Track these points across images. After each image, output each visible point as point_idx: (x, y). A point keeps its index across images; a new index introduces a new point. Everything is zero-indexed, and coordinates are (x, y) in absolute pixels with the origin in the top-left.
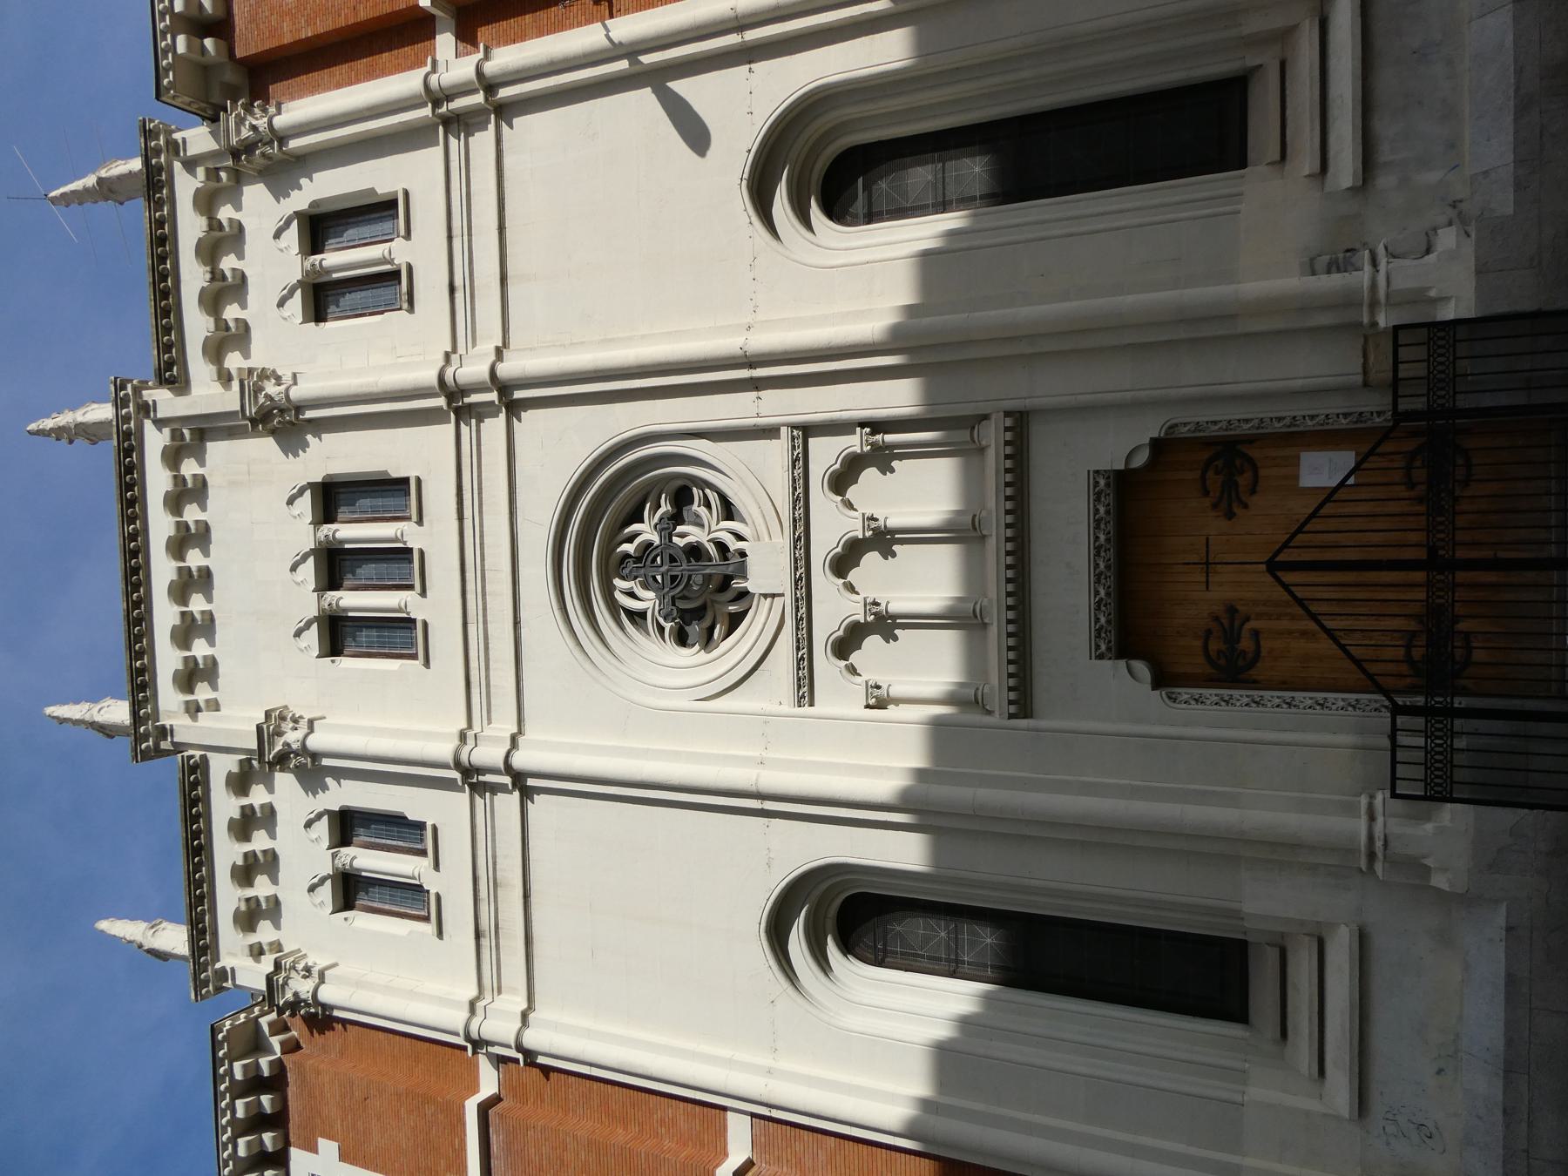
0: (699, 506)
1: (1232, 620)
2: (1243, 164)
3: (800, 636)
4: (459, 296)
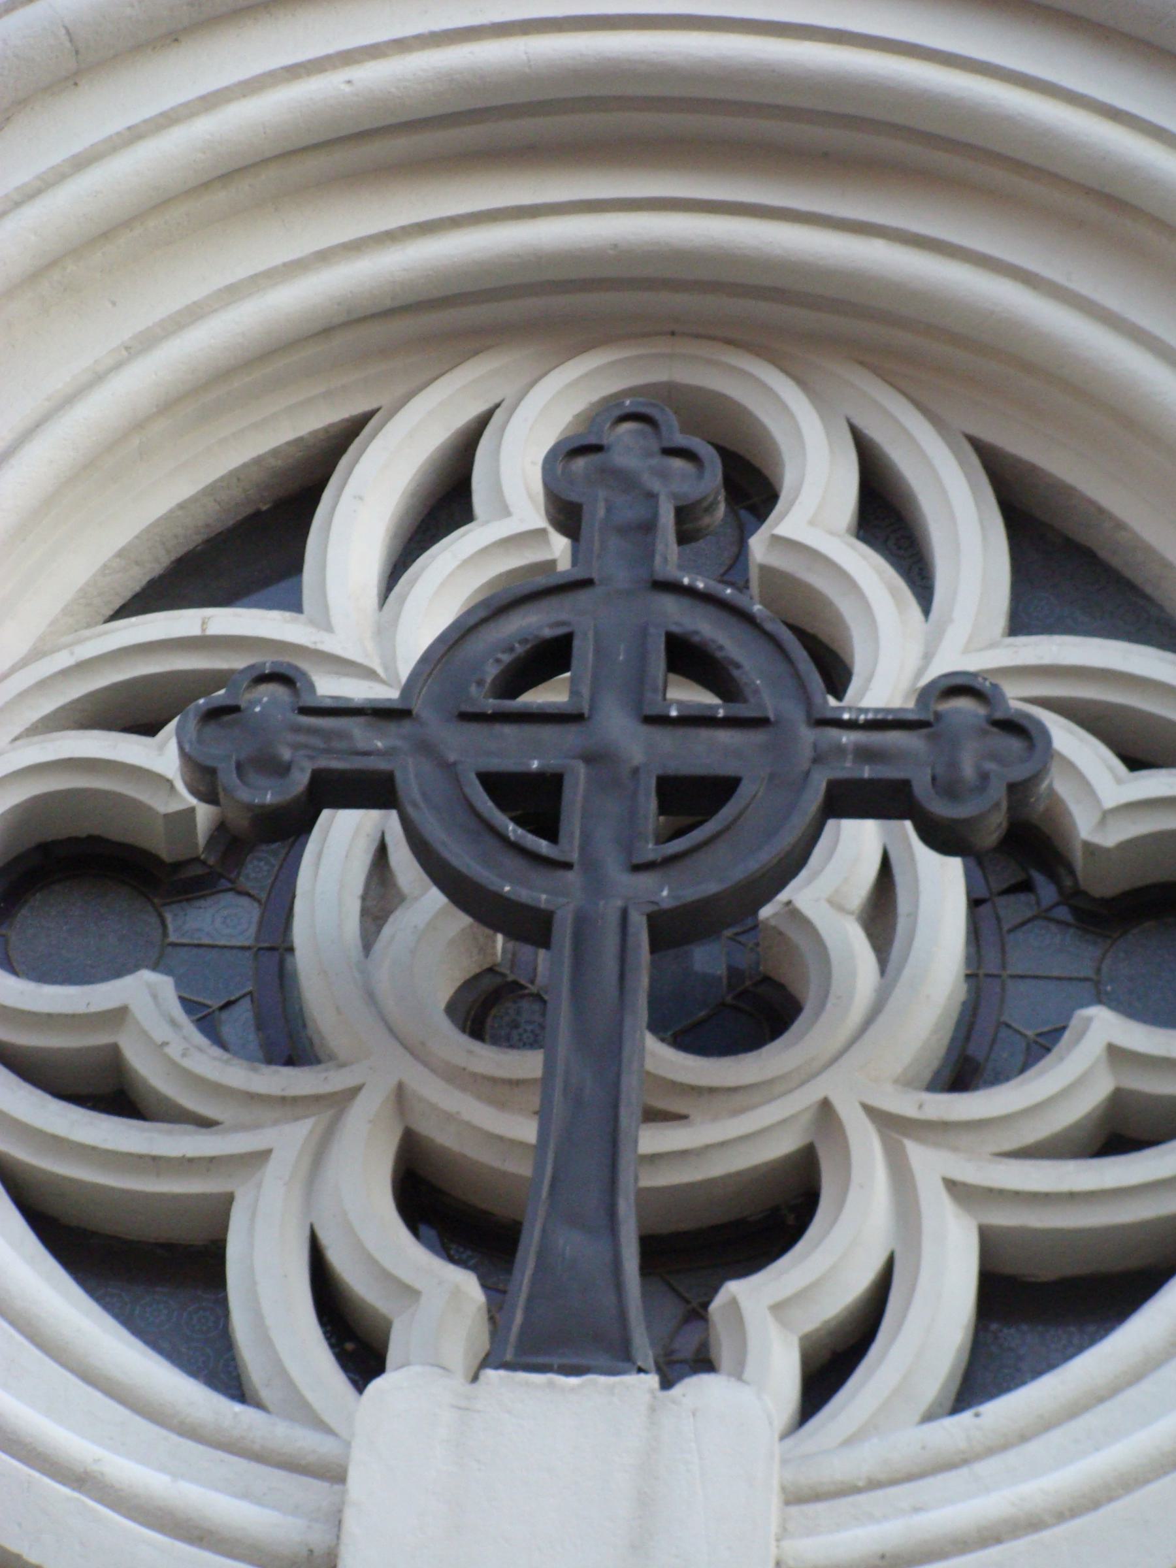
0: (1116, 1054)
3: (262, 864)
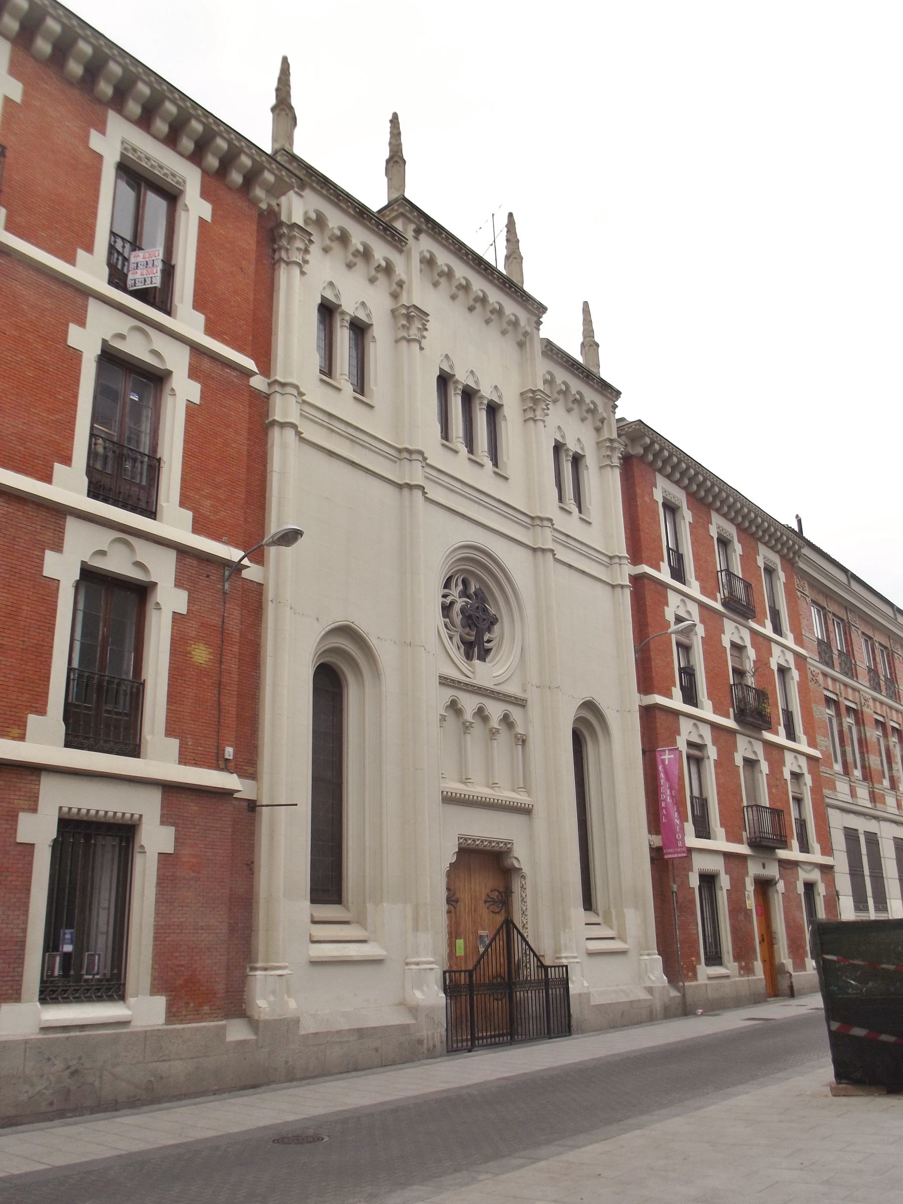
1: (489, 902)
2: (313, 901)
4: (325, 418)
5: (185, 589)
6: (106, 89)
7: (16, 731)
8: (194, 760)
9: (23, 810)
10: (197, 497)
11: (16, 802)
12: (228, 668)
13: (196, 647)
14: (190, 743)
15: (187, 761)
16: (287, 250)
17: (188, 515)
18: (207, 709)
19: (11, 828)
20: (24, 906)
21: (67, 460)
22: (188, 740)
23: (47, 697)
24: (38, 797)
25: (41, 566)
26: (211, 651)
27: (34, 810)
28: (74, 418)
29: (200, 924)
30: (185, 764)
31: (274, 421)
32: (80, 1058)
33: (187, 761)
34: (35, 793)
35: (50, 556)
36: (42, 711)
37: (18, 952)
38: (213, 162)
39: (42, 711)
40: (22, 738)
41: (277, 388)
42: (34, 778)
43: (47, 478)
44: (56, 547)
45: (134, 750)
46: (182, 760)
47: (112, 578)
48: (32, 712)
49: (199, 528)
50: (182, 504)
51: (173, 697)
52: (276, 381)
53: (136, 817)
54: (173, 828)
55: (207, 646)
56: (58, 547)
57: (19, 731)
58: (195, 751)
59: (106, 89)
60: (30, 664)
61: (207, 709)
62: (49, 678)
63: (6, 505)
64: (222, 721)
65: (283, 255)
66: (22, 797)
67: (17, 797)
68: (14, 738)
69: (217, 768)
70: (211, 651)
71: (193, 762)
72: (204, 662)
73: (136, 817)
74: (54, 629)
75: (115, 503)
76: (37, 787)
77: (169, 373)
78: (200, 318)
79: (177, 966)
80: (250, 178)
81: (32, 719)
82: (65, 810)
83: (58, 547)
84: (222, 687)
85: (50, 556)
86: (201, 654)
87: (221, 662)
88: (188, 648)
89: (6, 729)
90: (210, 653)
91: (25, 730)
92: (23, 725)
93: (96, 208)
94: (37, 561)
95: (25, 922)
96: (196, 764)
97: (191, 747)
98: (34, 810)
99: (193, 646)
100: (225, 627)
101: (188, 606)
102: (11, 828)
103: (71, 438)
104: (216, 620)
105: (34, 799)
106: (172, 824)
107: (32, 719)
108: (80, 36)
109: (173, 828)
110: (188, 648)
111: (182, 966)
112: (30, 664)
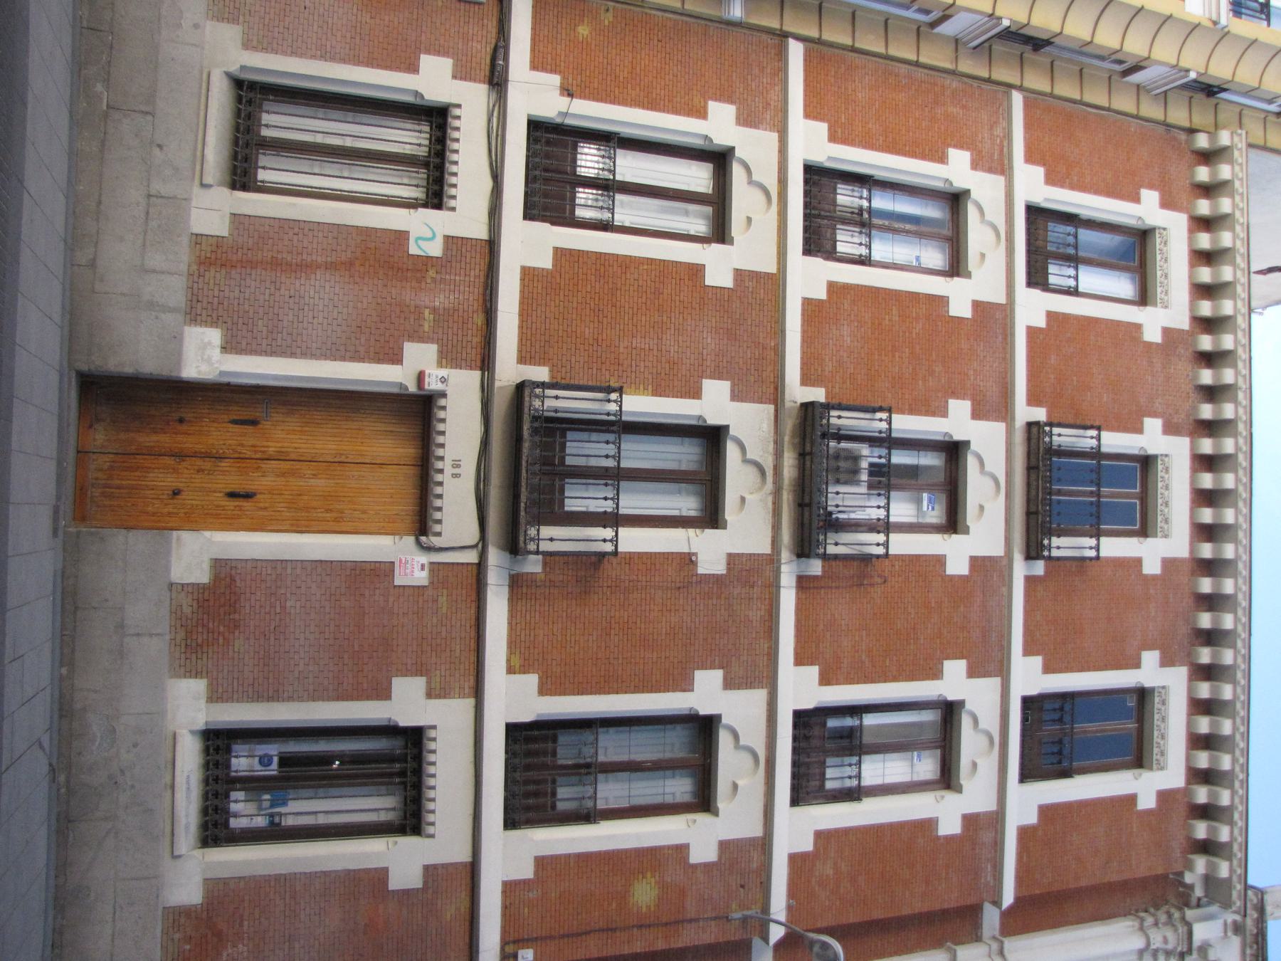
5: (720, 857)
6: (1205, 655)
7: (516, 662)
8: (510, 904)
9: (429, 682)
10: (833, 855)
11: (438, 672)
12: (635, 937)
13: (653, 885)
14: (531, 895)
15: (508, 894)
16: (1156, 924)
17: (807, 845)
18: (578, 914)
19: (407, 670)
20: (317, 695)
21: (825, 680)
22: (535, 892)
23: (560, 694)
24: (445, 697)
25: (704, 667)
26: (652, 909)
27: (429, 695)
28: (873, 681)
29: (297, 946)
30: (504, 892)
31: (955, 951)
32: (133, 787)
33: (508, 894)
34: (450, 694)
35: (716, 676)
36: (543, 690)
37: (265, 694)
38: (1202, 795)
39: (543, 690)
40: (510, 670)
41: (995, 946)
42: (467, 691)
43: (800, 660)
44: (729, 682)
45: (511, 823)
46: (508, 886)
47: (710, 764)
48: (540, 678)
49: (796, 860)
50: (819, 835)
51: (585, 861)
52: (1002, 943)
53: (452, 203)
54: (420, 886)
55: (657, 900)
56: (729, 684)
57: (517, 666)
58: (522, 906)
59: (1205, 655)
60: (594, 670)
61: (578, 914)
62: (582, 694)
63: (758, 619)
64: (566, 940)
65: (1149, 920)
66: (443, 678)
67: (443, 674)
68: (508, 661)
69: (504, 943)
70: (652, 909)
71: (508, 904)
72: (635, 899)
73: (452, 203)
74: (638, 692)
75: (796, 751)
76: (457, 696)
77: (959, 789)
78: (1032, 818)
79: (242, 916)
80: (1207, 847)
81: (532, 680)
82: (456, 112)
83: (729, 684)
84: (610, 933)
85: (716, 676)
86: (644, 894)
87: (640, 927)
88: (649, 875)
89: (518, 650)
90: (648, 907)
91: (520, 673)
92: (524, 669)
93: (1089, 669)
94: (709, 662)
95: (300, 699)
96: (506, 907)
97: (526, 897)
98: (429, 695)
99: (653, 880)
100: (685, 924)
101: (700, 864)
102: (407, 670)
103: (850, 681)
104: (691, 912)
105: (443, 694)
106: (425, 883)
107: (532, 680)
108: (1235, 613)
109: (420, 886)
110: (649, 875)
111: (241, 925)
112: (594, 670)
